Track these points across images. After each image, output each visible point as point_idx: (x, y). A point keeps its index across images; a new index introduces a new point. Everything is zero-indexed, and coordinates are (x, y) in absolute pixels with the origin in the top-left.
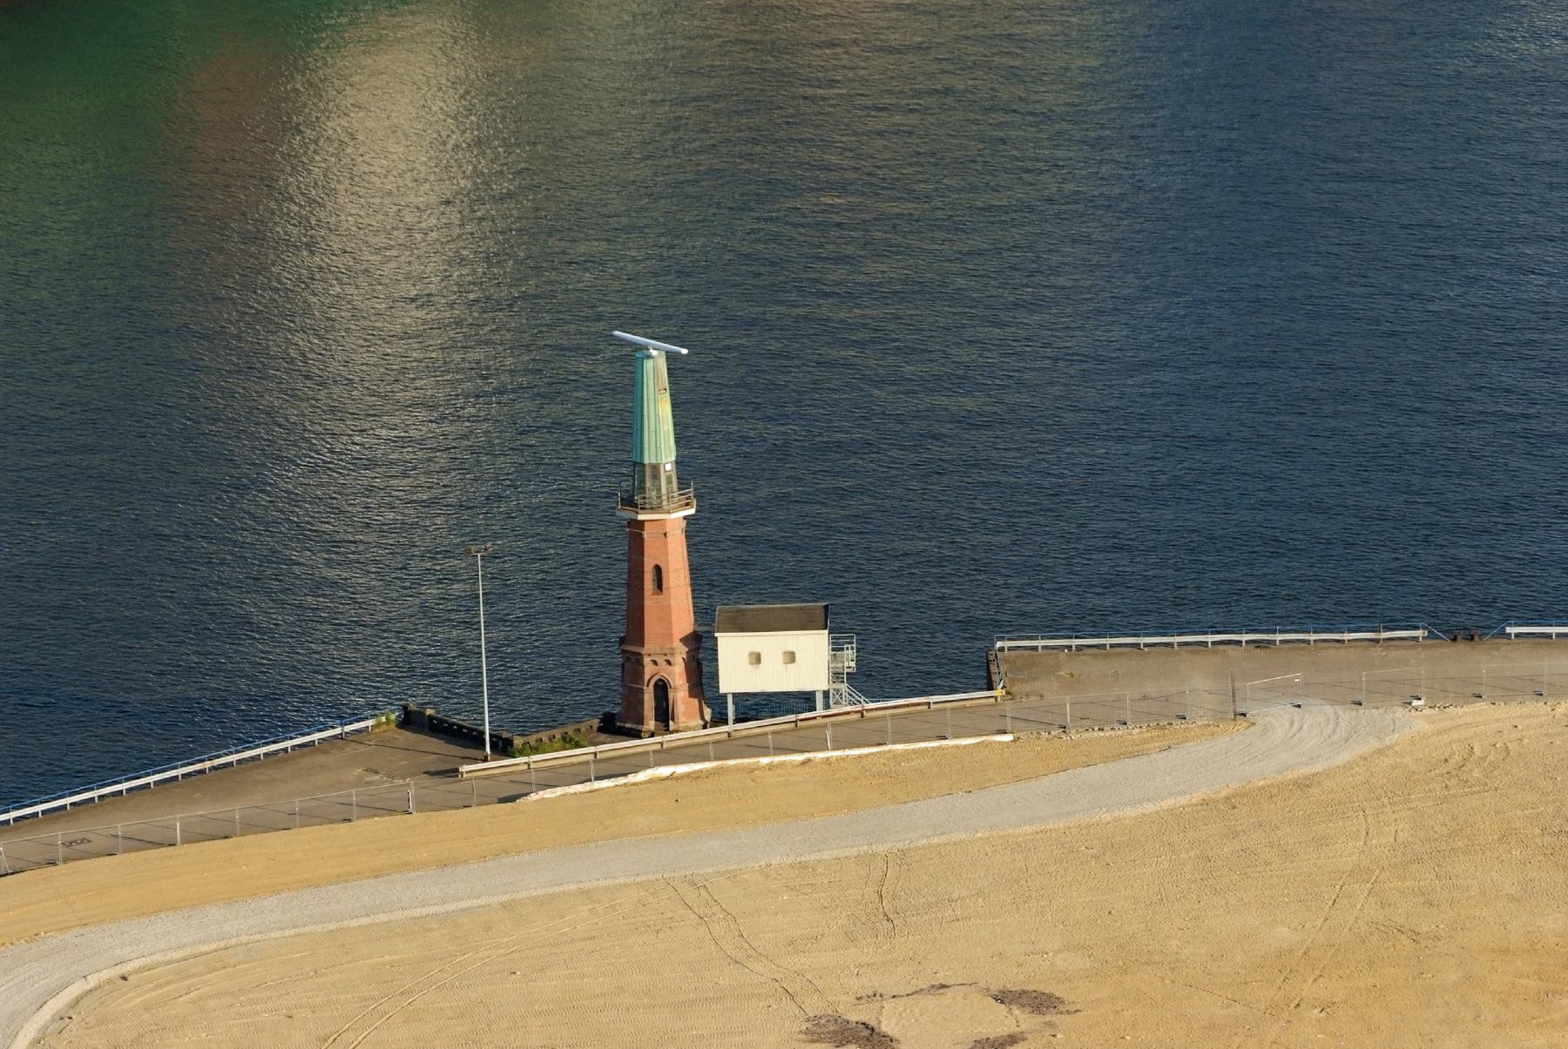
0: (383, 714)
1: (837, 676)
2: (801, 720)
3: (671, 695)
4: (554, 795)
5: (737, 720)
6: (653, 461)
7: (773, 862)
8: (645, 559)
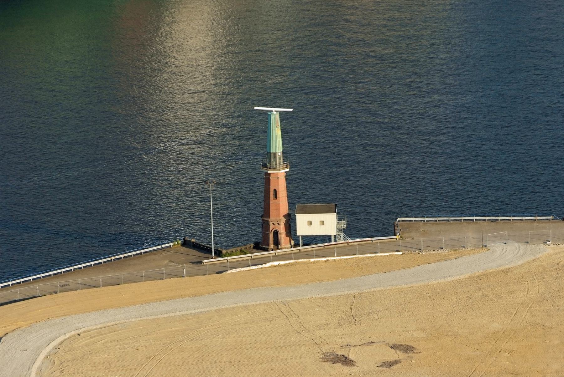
1: (339, 230)
2: (326, 246)
3: (279, 236)
4: (236, 271)
5: (303, 245)
6: (274, 152)
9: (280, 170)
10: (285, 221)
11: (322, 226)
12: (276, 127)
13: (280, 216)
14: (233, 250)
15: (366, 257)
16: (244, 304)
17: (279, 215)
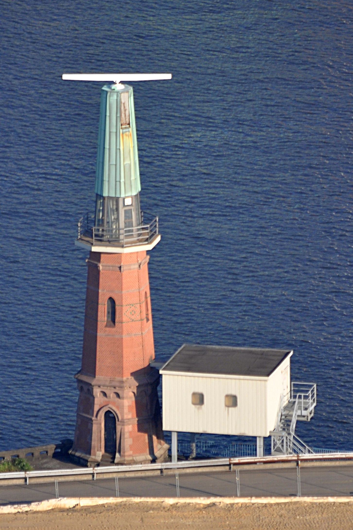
2: (235, 464)
3: (119, 428)
5: (179, 459)
9: (123, 247)
10: (138, 387)
12: (119, 124)
13: (121, 374)
17: (120, 369)
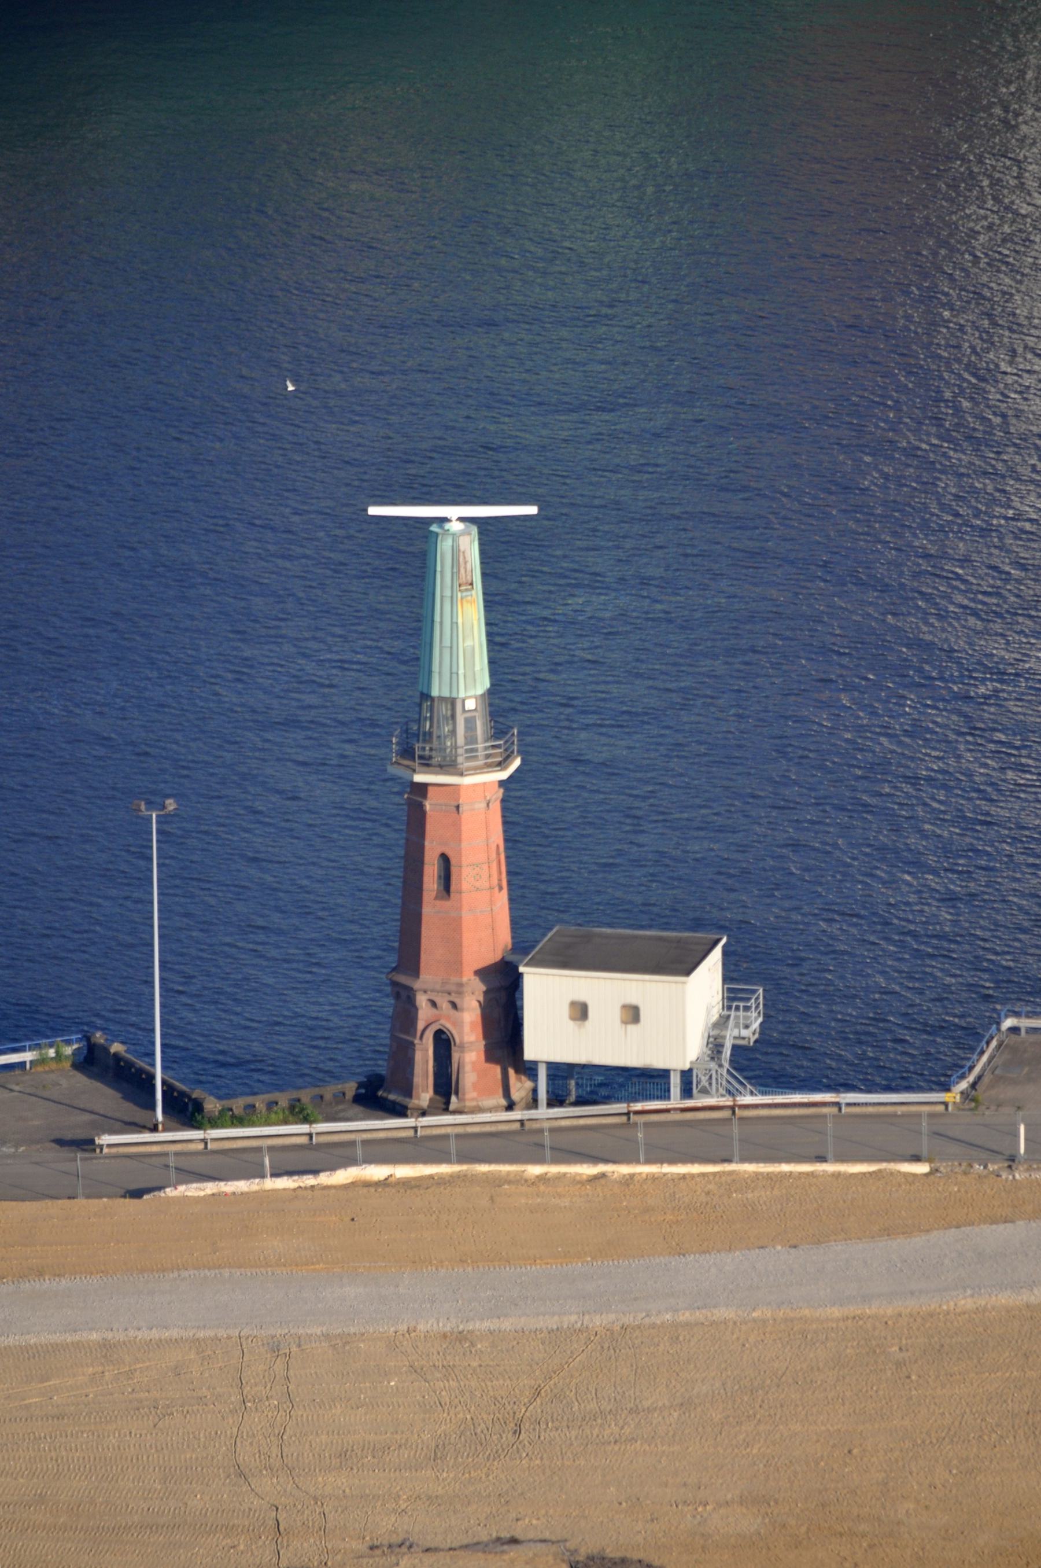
0: (51, 1046)
1: (715, 1047)
3: (455, 1056)
4: (202, 1194)
5: (550, 1104)
6: (446, 693)
7: (421, 1327)
8: (427, 843)
10: (486, 993)
11: (631, 1028)
12: (456, 585)
13: (460, 972)
14: (260, 1102)
15: (769, 1176)
16: (109, 1335)
